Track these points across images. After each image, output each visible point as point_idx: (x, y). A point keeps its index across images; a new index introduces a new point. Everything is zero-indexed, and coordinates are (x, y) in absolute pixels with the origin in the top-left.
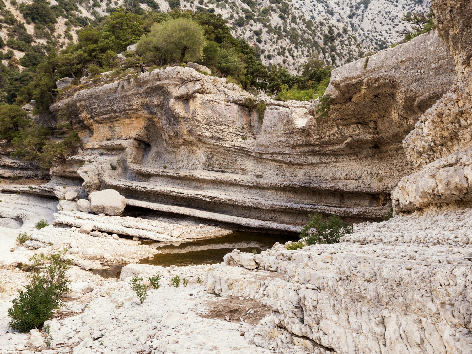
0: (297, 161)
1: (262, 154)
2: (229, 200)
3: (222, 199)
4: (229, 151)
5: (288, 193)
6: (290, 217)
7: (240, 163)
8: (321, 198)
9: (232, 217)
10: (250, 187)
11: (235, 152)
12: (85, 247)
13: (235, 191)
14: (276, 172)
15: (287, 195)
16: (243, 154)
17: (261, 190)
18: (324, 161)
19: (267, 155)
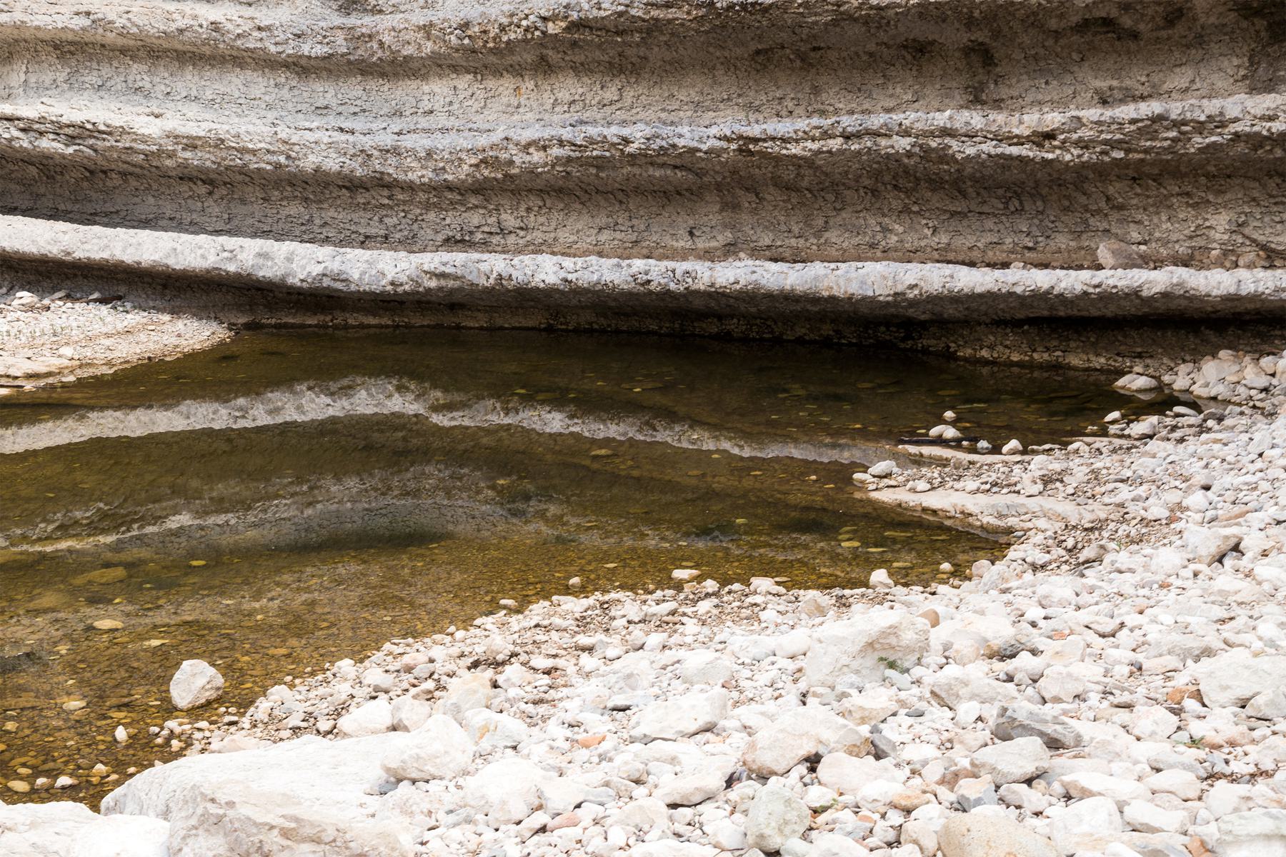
2: (192, 144)
3: (144, 139)
6: (602, 220)
8: (816, 90)
9: (223, 239)
10: (302, 68)
12: (596, 759)
13: (209, 94)
15: (564, 95)
17: (372, 84)
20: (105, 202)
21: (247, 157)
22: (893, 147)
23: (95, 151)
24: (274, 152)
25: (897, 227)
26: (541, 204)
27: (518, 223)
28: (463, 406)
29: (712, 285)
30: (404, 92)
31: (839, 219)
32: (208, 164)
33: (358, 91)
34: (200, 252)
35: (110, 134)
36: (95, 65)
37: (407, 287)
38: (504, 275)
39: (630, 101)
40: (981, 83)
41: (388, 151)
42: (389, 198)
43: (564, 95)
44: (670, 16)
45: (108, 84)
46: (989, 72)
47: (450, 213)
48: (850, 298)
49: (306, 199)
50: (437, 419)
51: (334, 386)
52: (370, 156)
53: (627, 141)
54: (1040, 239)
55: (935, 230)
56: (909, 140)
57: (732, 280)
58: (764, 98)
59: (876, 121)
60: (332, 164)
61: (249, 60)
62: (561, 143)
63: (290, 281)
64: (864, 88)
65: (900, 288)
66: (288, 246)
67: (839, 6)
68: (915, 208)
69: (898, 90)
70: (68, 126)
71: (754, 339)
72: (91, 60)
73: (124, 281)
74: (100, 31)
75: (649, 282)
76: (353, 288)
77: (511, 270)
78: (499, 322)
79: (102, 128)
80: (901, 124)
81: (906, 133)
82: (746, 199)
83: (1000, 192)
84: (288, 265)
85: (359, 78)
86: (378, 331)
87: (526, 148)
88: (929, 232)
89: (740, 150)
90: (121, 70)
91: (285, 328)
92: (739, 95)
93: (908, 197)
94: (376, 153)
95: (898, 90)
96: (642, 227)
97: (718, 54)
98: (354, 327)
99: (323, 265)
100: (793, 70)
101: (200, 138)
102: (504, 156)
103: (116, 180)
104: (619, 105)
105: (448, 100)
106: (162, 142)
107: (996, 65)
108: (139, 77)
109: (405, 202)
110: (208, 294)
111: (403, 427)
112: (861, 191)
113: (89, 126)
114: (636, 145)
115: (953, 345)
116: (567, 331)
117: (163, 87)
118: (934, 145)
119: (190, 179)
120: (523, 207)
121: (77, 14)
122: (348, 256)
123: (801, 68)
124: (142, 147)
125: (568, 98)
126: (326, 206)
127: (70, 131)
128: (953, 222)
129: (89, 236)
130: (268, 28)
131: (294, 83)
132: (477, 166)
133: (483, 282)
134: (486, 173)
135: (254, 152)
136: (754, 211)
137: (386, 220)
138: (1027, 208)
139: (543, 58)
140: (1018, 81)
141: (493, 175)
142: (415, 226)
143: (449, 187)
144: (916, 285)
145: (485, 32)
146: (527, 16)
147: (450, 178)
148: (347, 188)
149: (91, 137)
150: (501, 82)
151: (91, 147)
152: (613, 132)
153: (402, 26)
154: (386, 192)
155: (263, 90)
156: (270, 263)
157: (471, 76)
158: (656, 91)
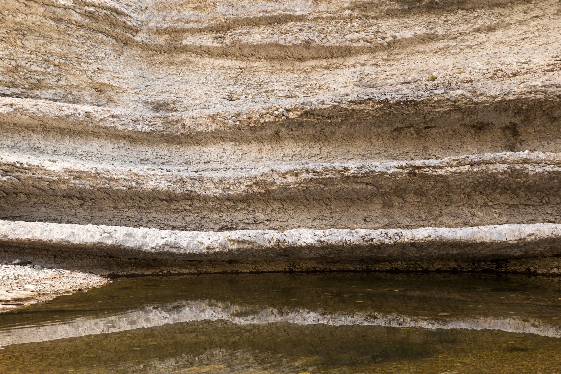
0: (333, 41)
1: (175, 33)
3: (50, 173)
4: (59, 20)
5: (292, 144)
6: (315, 214)
7: (95, 66)
8: (425, 149)
11: (82, 26)
13: (79, 152)
14: (230, 88)
15: (289, 152)
16: (107, 35)
17: (173, 148)
18: (440, 31)
19: (197, 36)
20: (13, 211)
21: (112, 183)
22: (496, 169)
23: (19, 179)
24: (128, 181)
25: (479, 213)
26: (281, 206)
27: (266, 218)
28: (254, 312)
29: (413, 239)
30: (191, 152)
31: (447, 211)
32: (88, 187)
33: (165, 152)
34: (89, 234)
35: (30, 170)
36: (9, 135)
37: (217, 250)
38: (281, 240)
39: (325, 154)
40: (513, 144)
41: (195, 179)
42: (190, 206)
43: (289, 152)
44: (363, 108)
45: (18, 145)
46: (516, 139)
47: (225, 214)
48: (492, 243)
49: (139, 207)
50: (237, 321)
51: (169, 306)
52: (185, 182)
53: (346, 169)
54: (557, 217)
56: (506, 165)
57: (426, 235)
58: (398, 152)
59: (488, 156)
60: (163, 186)
61: (103, 134)
62: (307, 171)
63: (144, 249)
64: (451, 147)
65: (523, 236)
66: (142, 231)
67: (455, 102)
68: (490, 204)
69: (469, 148)
70: (5, 165)
71: (413, 272)
72: (7, 132)
73: (30, 254)
74: (19, 115)
75: (372, 239)
76: (182, 251)
77: (285, 238)
78: (261, 269)
79: (26, 166)
80: (501, 158)
81: (504, 162)
82: (397, 201)
83: (538, 193)
84: (143, 240)
85: (166, 144)
86: (188, 276)
87: (284, 175)
88: (497, 216)
89: (410, 173)
90: (26, 138)
91: (137, 277)
92: (385, 151)
93: (487, 198)
94: (189, 181)
95: (469, 148)
96: (338, 218)
97: (375, 130)
99: (165, 239)
100: (412, 139)
101: (85, 172)
102: (270, 180)
103: (23, 197)
104: (319, 157)
105: (219, 155)
106: (61, 174)
107: (519, 135)
108: (37, 142)
109: (199, 208)
110: (82, 260)
111: (195, 330)
112: (462, 196)
113: (18, 165)
114: (352, 171)
115: (532, 268)
116: (302, 272)
117: (52, 148)
118: (518, 168)
119: (69, 197)
120: (269, 209)
121: (5, 105)
123: (416, 138)
124: (48, 177)
125: (291, 153)
126: (150, 211)
127: (5, 168)
128: (510, 210)
129: (18, 226)
130: (118, 116)
131: (128, 147)
132: (250, 186)
133: (266, 244)
134: (255, 189)
135: (116, 180)
136: (400, 208)
137: (186, 218)
138: (552, 201)
139: (277, 133)
140: (532, 143)
141: (259, 191)
142: (203, 221)
143: (229, 198)
144: (533, 234)
145: (249, 118)
146: (277, 109)
147: (232, 193)
148: (166, 201)
149: (17, 171)
150: (250, 146)
151: (17, 177)
152: (337, 165)
153: (198, 116)
154: (189, 203)
155: (111, 150)
156: (132, 239)
157: (233, 143)
158: (340, 149)
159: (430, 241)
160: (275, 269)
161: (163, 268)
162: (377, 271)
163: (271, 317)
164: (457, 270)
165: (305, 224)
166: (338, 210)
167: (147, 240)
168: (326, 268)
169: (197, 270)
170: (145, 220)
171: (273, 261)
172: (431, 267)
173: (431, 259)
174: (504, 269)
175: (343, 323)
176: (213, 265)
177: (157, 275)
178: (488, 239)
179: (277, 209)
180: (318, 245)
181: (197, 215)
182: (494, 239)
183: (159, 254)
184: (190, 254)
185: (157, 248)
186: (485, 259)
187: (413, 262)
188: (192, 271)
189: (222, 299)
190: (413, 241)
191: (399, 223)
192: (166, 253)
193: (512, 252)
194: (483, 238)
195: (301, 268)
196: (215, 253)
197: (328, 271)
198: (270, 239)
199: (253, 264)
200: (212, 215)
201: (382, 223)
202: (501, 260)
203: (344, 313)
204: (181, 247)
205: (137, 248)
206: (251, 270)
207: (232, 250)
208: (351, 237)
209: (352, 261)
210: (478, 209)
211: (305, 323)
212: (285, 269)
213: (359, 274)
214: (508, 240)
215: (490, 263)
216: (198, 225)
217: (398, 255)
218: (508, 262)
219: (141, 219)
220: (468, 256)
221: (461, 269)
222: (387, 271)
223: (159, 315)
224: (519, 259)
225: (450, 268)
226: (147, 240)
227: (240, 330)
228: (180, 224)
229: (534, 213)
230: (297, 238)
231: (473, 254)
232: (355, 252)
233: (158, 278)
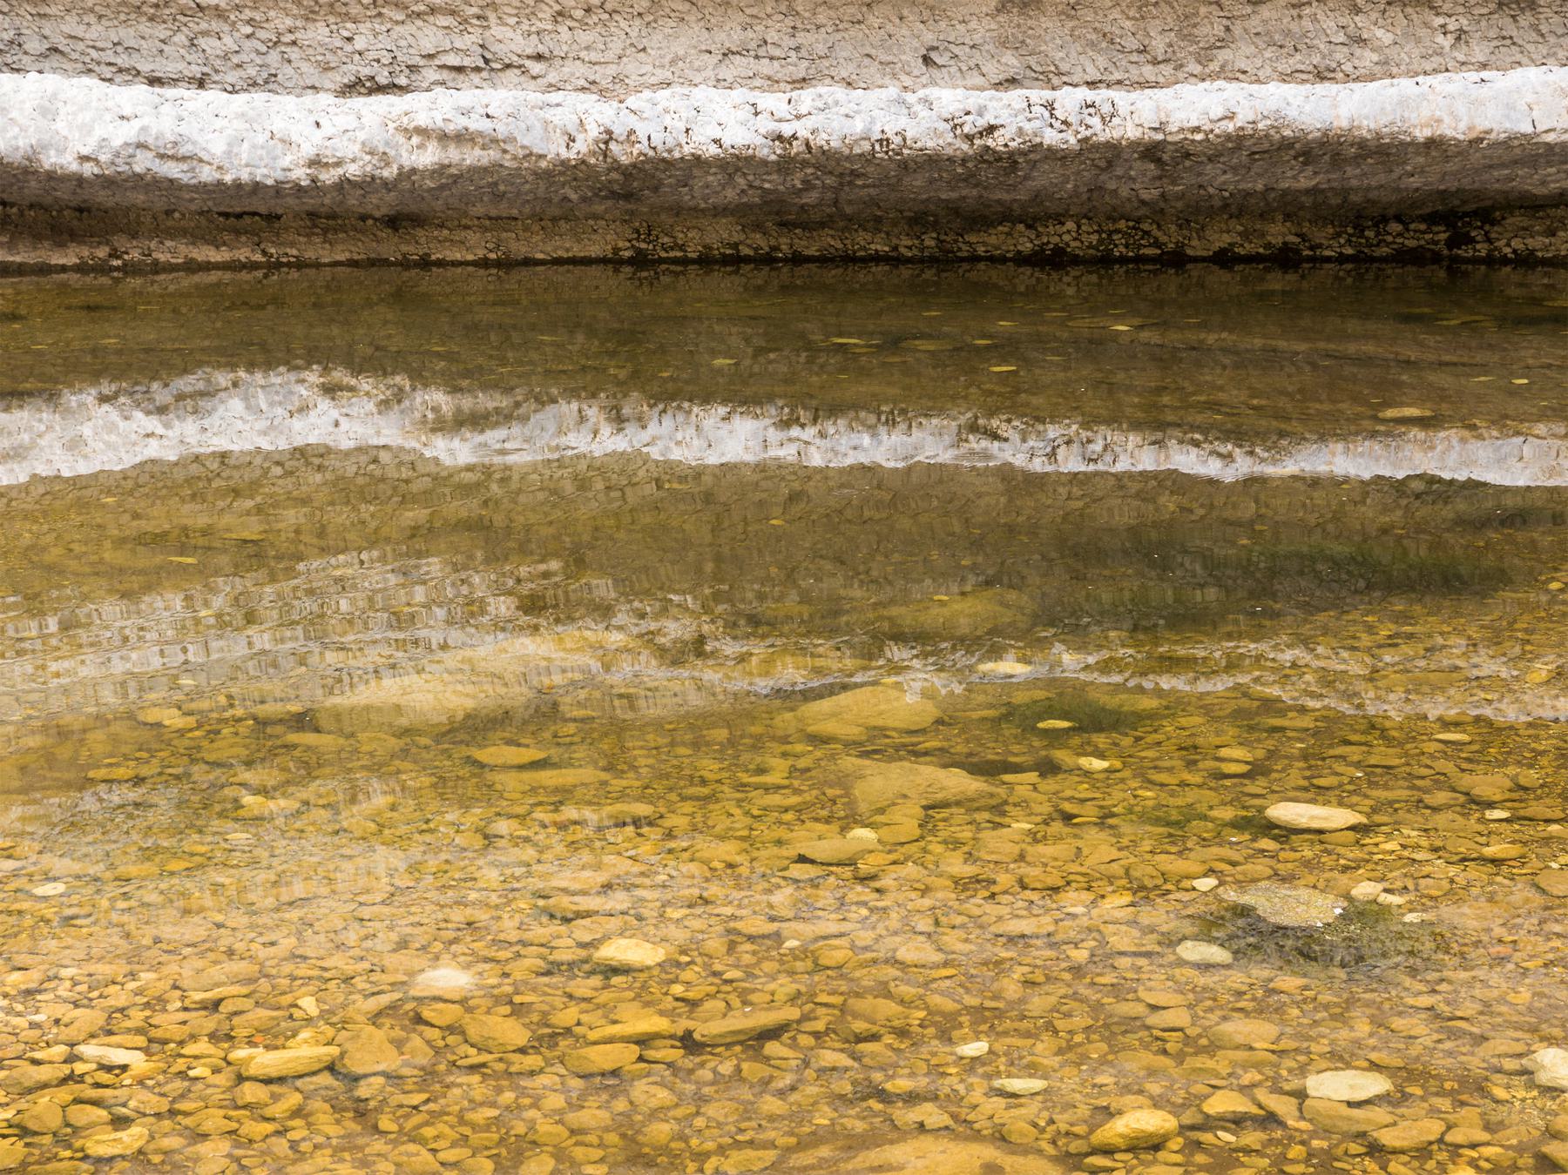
6: (731, 34)
25: (1380, 33)
31: (1254, 23)
37: (353, 170)
47: (363, 28)
51: (161, 395)
55: (1460, 35)
57: (1217, 112)
71: (1123, 260)
75: (991, 129)
76: (207, 175)
77: (632, 122)
86: (227, 276)
88: (1446, 42)
96: (821, 49)
98: (172, 268)
99: (136, 124)
116: (685, 262)
122: (190, 106)
133: (555, 149)
137: (202, 42)
142: (274, 57)
159: (1228, 137)
160: (577, 251)
161: (121, 242)
162: (978, 259)
163: (574, 436)
164: (1298, 252)
165: (689, 73)
166: (821, 19)
167: (61, 126)
168: (776, 248)
169: (264, 253)
170: (34, 45)
171: (567, 219)
172: (1195, 243)
173: (1197, 213)
174: (1482, 249)
175: (864, 459)
176: (325, 231)
177: (102, 269)
178: (1462, 126)
179: (579, 14)
180: (769, 152)
181: (249, 30)
182: (1486, 125)
183: (108, 182)
184: (238, 185)
185: (103, 158)
186: (1402, 213)
187: (1122, 225)
188: (243, 254)
189: (374, 363)
190: (1160, 137)
191: (1059, 74)
192: (140, 182)
193: (1532, 182)
194: (1439, 121)
195: (682, 248)
196: (344, 184)
197: (785, 260)
198: (572, 130)
199: (486, 230)
200: (310, 34)
201: (994, 71)
202: (1466, 214)
203: (872, 419)
204: (202, 155)
205: (17, 158)
206: (481, 253)
207: (414, 171)
208: (903, 122)
209: (878, 220)
210: (1374, 15)
211: (713, 459)
212: (616, 250)
213: (906, 272)
214: (1540, 128)
215: (1423, 227)
216: (252, 71)
217: (1076, 193)
218: (1493, 223)
219: (16, 43)
220: (1345, 200)
221: (1312, 248)
222: (1022, 260)
223: (122, 424)
224: (1542, 207)
225: (1268, 246)
226: (61, 126)
227: (443, 481)
228: (181, 66)
229: (977, 142)
230: (682, 126)
231: (1369, 189)
232: (907, 180)
233: (104, 280)
